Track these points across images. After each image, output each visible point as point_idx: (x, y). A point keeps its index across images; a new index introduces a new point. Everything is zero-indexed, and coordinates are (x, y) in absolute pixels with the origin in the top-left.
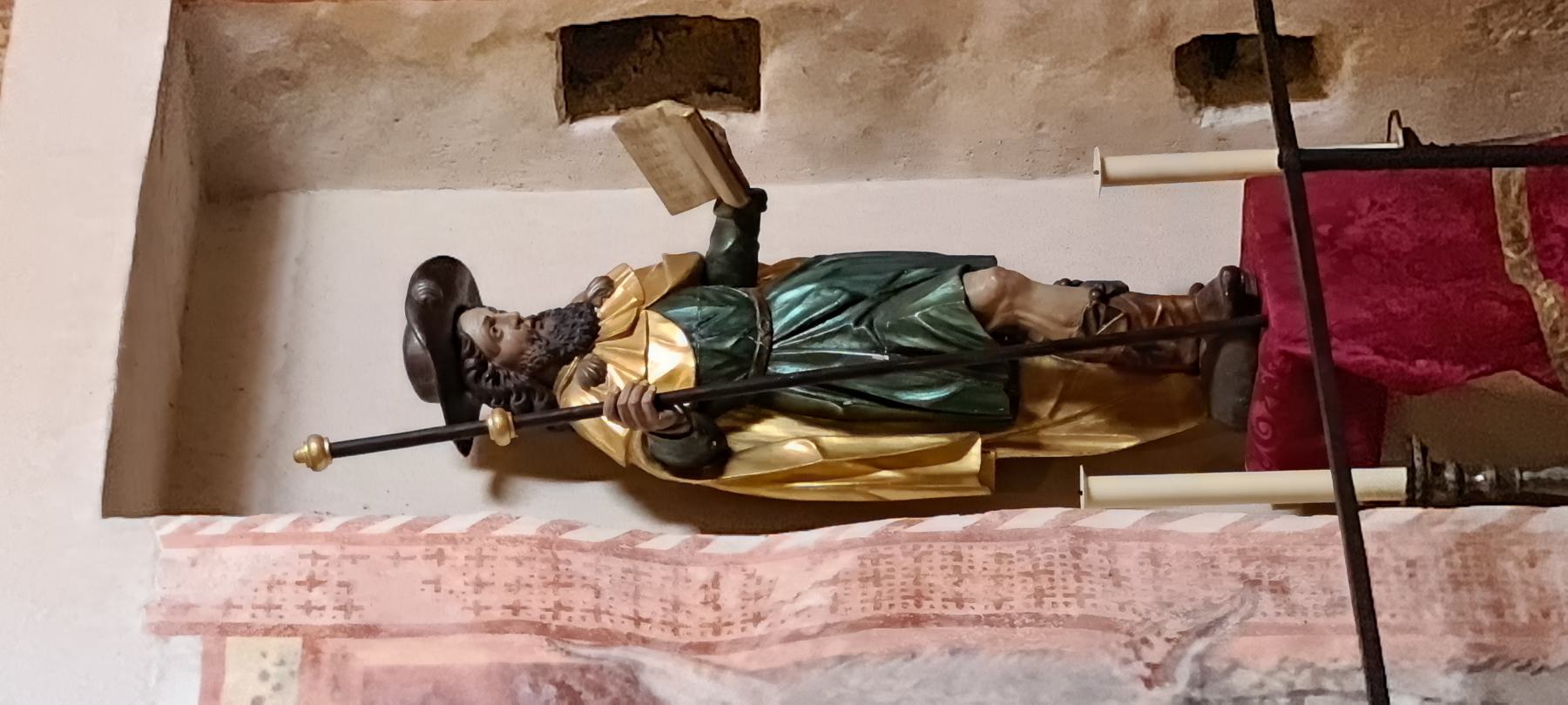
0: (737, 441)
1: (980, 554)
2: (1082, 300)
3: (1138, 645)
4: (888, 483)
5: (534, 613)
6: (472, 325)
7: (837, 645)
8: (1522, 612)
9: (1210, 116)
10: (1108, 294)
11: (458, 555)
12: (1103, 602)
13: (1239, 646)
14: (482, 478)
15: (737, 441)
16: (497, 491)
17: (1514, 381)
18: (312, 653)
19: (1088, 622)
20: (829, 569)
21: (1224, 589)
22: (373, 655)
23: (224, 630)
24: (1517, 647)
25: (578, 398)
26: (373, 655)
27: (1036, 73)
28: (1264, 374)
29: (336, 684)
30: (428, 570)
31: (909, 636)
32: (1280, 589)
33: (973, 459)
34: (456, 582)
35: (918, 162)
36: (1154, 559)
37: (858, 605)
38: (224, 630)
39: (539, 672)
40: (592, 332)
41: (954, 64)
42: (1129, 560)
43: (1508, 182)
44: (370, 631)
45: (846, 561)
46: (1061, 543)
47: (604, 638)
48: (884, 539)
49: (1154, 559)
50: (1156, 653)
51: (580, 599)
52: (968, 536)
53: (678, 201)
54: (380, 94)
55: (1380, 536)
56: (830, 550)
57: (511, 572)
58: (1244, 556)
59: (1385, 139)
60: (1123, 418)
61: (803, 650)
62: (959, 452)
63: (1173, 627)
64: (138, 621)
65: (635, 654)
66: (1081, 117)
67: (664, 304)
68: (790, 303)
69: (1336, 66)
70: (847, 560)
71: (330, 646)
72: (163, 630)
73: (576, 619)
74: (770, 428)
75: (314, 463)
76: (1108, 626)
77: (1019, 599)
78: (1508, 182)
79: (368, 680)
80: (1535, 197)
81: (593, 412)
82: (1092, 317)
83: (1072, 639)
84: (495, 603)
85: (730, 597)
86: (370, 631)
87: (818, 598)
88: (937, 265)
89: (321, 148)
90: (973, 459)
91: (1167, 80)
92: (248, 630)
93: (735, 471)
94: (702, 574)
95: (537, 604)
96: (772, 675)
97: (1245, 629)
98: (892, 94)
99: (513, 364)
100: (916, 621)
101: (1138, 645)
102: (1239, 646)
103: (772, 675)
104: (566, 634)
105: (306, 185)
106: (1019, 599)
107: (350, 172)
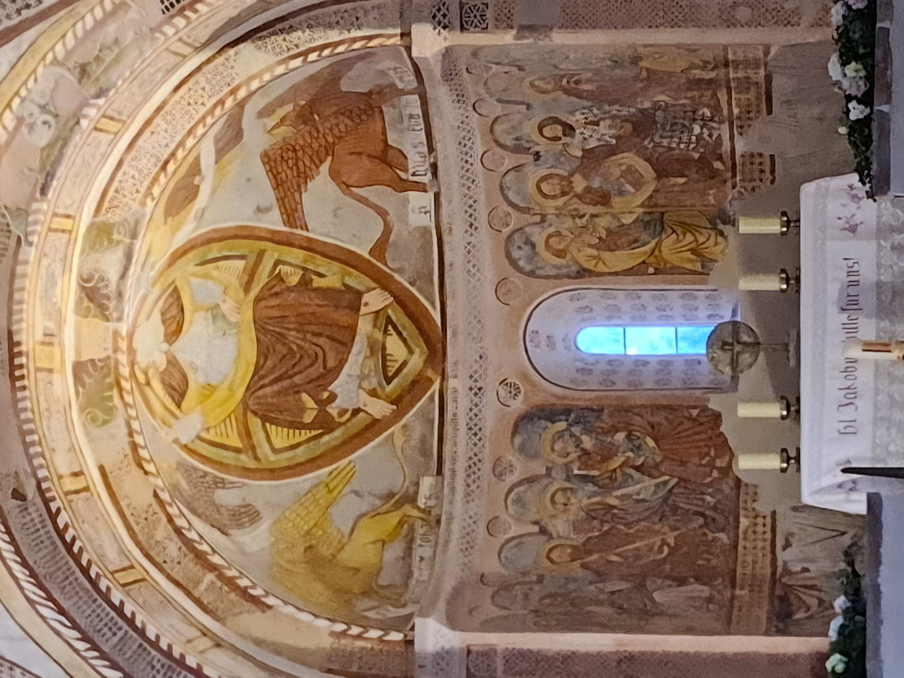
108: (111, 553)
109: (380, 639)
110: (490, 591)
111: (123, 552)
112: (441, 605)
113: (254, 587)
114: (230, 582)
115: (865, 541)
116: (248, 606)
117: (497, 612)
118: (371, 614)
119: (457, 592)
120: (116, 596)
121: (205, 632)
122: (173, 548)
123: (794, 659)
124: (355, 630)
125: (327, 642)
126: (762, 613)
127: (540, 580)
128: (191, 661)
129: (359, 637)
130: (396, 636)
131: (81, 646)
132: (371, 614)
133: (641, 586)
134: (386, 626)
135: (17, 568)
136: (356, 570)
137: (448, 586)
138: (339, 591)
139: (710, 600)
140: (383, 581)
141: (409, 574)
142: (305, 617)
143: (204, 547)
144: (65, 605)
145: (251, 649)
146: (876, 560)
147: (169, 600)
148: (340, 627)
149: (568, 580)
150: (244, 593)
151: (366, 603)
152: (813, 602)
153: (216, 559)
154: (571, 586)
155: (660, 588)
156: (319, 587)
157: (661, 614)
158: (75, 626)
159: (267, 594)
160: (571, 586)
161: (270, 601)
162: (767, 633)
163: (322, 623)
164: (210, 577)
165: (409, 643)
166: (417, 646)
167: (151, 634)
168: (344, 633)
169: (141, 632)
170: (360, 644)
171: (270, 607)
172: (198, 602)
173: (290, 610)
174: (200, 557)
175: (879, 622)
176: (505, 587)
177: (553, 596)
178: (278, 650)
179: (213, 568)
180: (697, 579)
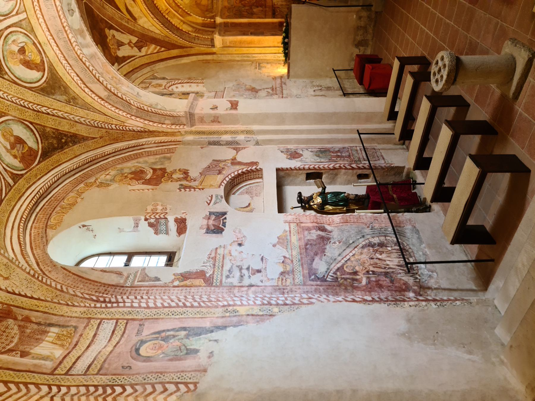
0: (325, 207)
1: (351, 217)
2: (354, 196)
3: (366, 225)
4: (338, 211)
5: (315, 221)
6: (303, 198)
7: (341, 224)
8: (398, 222)
9: (359, 180)
10: (356, 195)
11: (308, 217)
12: (363, 221)
13: (375, 225)
14: (303, 210)
15: (325, 207)
16: (304, 211)
17: (393, 203)
18: (297, 225)
19: (361, 223)
20: (339, 218)
21: (372, 220)
22: (303, 225)
23: (290, 223)
24: (398, 225)
25: (312, 204)
26: (303, 225)
27: (346, 176)
28: (370, 202)
29: (300, 227)
30: (306, 218)
31: (347, 224)
32: (377, 220)
33: (345, 209)
34: (308, 219)
35: (335, 184)
36: (366, 217)
37: (342, 221)
38: (290, 223)
39: (316, 226)
40: (313, 198)
41: (339, 176)
42: (364, 217)
43: (390, 186)
44: (302, 223)
45: (340, 217)
46: (358, 216)
47: (321, 224)
48: (343, 215)
49: (366, 217)
50: (368, 225)
51: (319, 220)
52: (350, 215)
53: (319, 187)
54: (291, 178)
55: (392, 216)
56: (339, 216)
57: (313, 218)
58: (374, 217)
59: (125, 73)
60: (357, 206)
61: (338, 225)
62: (344, 208)
63: (369, 223)
64: (283, 222)
65: (324, 225)
66: (349, 180)
67: (319, 196)
68: (329, 196)
69: (370, 177)
70: (340, 217)
71: (299, 224)
72: (285, 223)
73: (318, 222)
74: (327, 206)
75: (292, 209)
76: (363, 223)
77: (356, 221)
78: (390, 186)
79: (302, 227)
80: (392, 188)
81: (314, 205)
82: (355, 197)
83: (361, 224)
84: (312, 221)
85: (331, 220)
86: (302, 223)
87: (339, 220)
88: (342, 193)
89: (286, 183)
90: (345, 209)
91: (356, 178)
92: (292, 223)
93: (325, 210)
94: (328, 218)
95: (315, 221)
96: (336, 227)
97: (375, 223)
98: (334, 178)
99: (306, 201)
100: (347, 222)
101: (366, 225)
102: (375, 225)
103: (336, 227)
104: (318, 223)
105: (284, 186)
106: (356, 221)
107: (287, 185)
108: (164, 7)
109: (210, 21)
110: (227, 9)
111: (165, 6)
112: (219, 14)
113: (186, 9)
114: (184, 10)
115: (289, 13)
116: (187, 15)
117: (229, 14)
118: (208, 15)
119: (221, 10)
120: (167, 16)
121: (182, 21)
122: (174, 4)
123: (276, 23)
124: (206, 19)
125: (201, 22)
126: (270, 13)
127: (235, 7)
128: (180, 28)
129: (206, 20)
130: (212, 20)
131: (162, 26)
132: (208, 15)
133: (251, 8)
134: (211, 18)
135: (148, 11)
136: (204, 6)
137: (220, 9)
138: (201, 10)
139: (262, 11)
140: (209, 8)
141: (213, 7)
142: (197, 17)
143: (179, 4)
144: (158, 18)
145: (189, 23)
146: (291, 18)
147: (175, 15)
148: (203, 19)
149: (239, 7)
150: (187, 13)
151: (206, 13)
152: (278, 11)
153: (181, 6)
154: (240, 8)
155: (254, 8)
156: (198, 9)
157: (255, 14)
158: (160, 22)
159: (191, 13)
160: (240, 8)
161: (191, 14)
162: (272, 18)
163: (200, 18)
164: (180, 10)
165: (215, 21)
166: (216, 22)
167: (173, 23)
168: (204, 20)
169: (172, 23)
170: (207, 22)
171: (191, 15)
172: (179, 14)
173: (195, 16)
174: (178, 6)
175: (291, 28)
176: (229, 9)
177: (237, 10)
178: (193, 23)
179: (181, 8)
180: (260, 6)
